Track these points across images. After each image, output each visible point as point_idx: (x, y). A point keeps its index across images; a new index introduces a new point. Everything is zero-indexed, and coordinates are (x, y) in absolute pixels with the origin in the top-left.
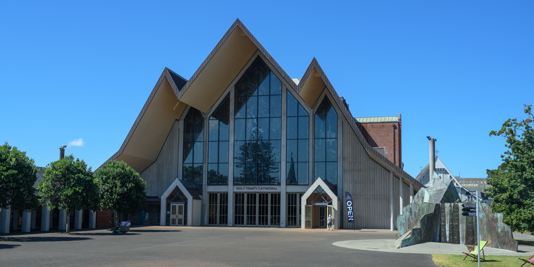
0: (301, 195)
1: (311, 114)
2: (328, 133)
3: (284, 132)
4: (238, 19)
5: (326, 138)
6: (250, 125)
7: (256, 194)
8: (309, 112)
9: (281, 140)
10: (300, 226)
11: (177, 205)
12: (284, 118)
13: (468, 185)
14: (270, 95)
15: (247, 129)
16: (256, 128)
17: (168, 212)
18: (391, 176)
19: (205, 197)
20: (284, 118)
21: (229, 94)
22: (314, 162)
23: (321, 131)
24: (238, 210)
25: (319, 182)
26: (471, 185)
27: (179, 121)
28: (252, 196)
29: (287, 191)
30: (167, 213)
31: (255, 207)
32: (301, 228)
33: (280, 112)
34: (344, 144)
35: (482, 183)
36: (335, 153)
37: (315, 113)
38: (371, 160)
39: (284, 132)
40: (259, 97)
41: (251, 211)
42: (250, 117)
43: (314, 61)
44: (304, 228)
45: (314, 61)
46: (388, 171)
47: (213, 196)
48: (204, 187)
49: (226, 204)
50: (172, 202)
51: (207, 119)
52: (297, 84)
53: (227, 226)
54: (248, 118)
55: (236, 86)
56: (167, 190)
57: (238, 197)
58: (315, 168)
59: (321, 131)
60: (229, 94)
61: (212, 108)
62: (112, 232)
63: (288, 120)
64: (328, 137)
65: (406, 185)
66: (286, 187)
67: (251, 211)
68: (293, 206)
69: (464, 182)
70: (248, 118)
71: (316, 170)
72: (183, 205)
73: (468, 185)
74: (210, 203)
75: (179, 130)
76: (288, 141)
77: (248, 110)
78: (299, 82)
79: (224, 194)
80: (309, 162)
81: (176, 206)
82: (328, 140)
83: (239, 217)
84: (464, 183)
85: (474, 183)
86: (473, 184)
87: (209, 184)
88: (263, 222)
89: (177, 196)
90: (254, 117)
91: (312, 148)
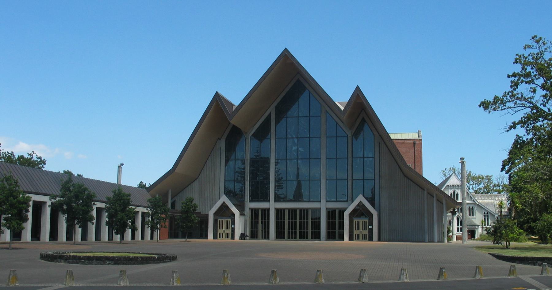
0: (345, 209)
1: (349, 135)
2: (365, 152)
3: (323, 152)
4: (286, 48)
5: (364, 158)
6: (291, 144)
7: (308, 210)
8: (347, 133)
9: (321, 158)
10: (341, 238)
11: (361, 221)
12: (323, 139)
13: (484, 201)
14: (310, 116)
15: (288, 148)
16: (296, 147)
17: (370, 227)
18: (426, 192)
19: (248, 212)
20: (323, 139)
21: (270, 115)
22: (353, 180)
23: (359, 150)
24: (280, 225)
25: (360, 199)
26: (486, 201)
27: (221, 139)
28: (292, 211)
29: (327, 207)
30: (372, 227)
31: (335, 222)
32: (343, 241)
33: (320, 133)
34: (381, 162)
35: (497, 199)
36: (372, 171)
37: (353, 133)
38: (405, 178)
39: (323, 152)
40: (299, 118)
41: (292, 226)
42: (290, 137)
43: (358, 89)
44: (348, 240)
45: (358, 89)
46: (422, 188)
47: (254, 212)
48: (246, 203)
49: (295, 220)
50: (355, 217)
51: (248, 138)
52: (343, 110)
53: (452, 236)
54: (289, 138)
55: (277, 107)
56: (215, 206)
57: (280, 212)
58: (354, 185)
59: (359, 150)
60: (270, 115)
61: (254, 127)
62: (537, 237)
63: (327, 140)
64: (365, 156)
65: (439, 201)
66: (326, 204)
67: (292, 226)
68: (295, 220)
69: (480, 198)
70: (289, 138)
71: (354, 187)
72: (367, 220)
73: (484, 201)
74: (252, 218)
75: (221, 148)
76: (327, 159)
77: (289, 131)
78: (344, 108)
79: (265, 210)
80: (347, 180)
81: (223, 221)
82: (366, 159)
83: (315, 229)
84: (480, 199)
85: (490, 199)
86: (489, 200)
87: (250, 201)
88: (304, 236)
89: (224, 211)
90: (294, 137)
91: (350, 167)
